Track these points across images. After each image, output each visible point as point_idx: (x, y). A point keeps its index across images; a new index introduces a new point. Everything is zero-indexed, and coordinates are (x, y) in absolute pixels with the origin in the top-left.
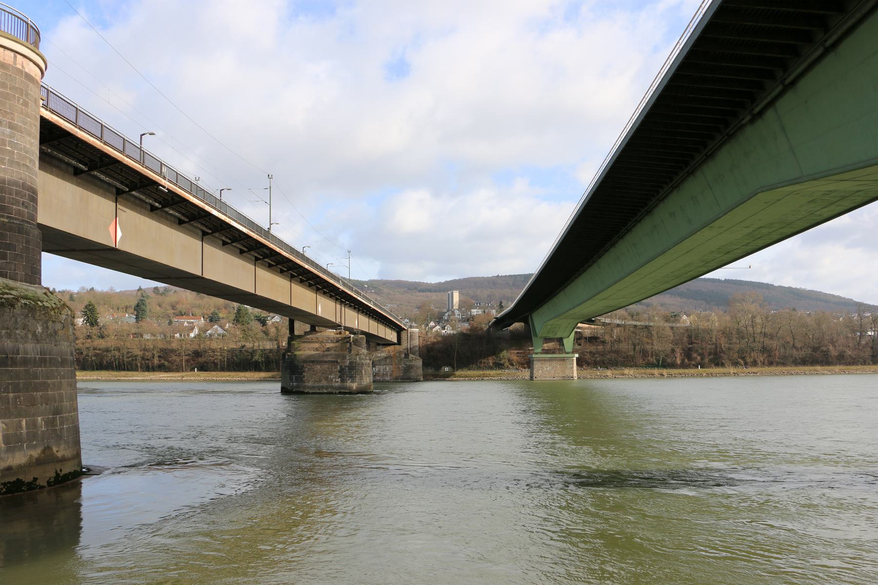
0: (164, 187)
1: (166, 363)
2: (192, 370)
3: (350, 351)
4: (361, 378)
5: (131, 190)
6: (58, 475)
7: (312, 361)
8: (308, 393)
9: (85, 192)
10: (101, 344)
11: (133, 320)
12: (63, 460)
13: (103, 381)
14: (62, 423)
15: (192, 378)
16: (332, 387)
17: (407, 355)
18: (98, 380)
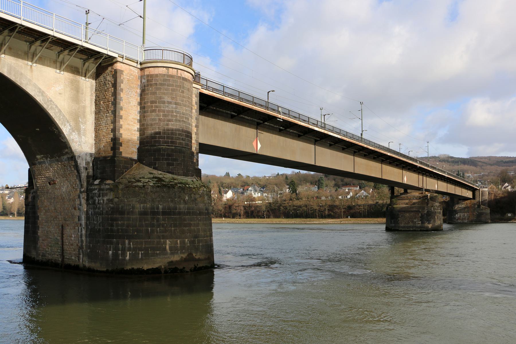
0: (280, 119)
1: (332, 213)
2: (347, 217)
3: (428, 204)
4: (435, 221)
5: (264, 122)
6: (196, 267)
7: (403, 211)
8: (401, 231)
9: (238, 126)
10: (297, 203)
11: (317, 189)
12: (199, 260)
13: (297, 224)
14: (199, 242)
15: (346, 222)
16: (416, 227)
17: (479, 206)
18: (295, 223)
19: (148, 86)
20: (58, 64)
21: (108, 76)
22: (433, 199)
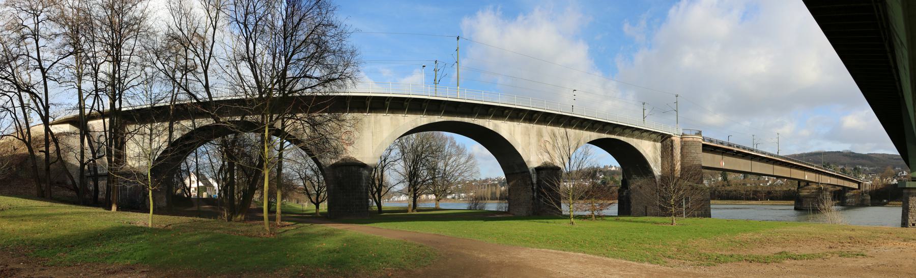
10: (728, 188)
19: (684, 145)
20: (650, 139)
21: (668, 141)
22: (826, 190)
